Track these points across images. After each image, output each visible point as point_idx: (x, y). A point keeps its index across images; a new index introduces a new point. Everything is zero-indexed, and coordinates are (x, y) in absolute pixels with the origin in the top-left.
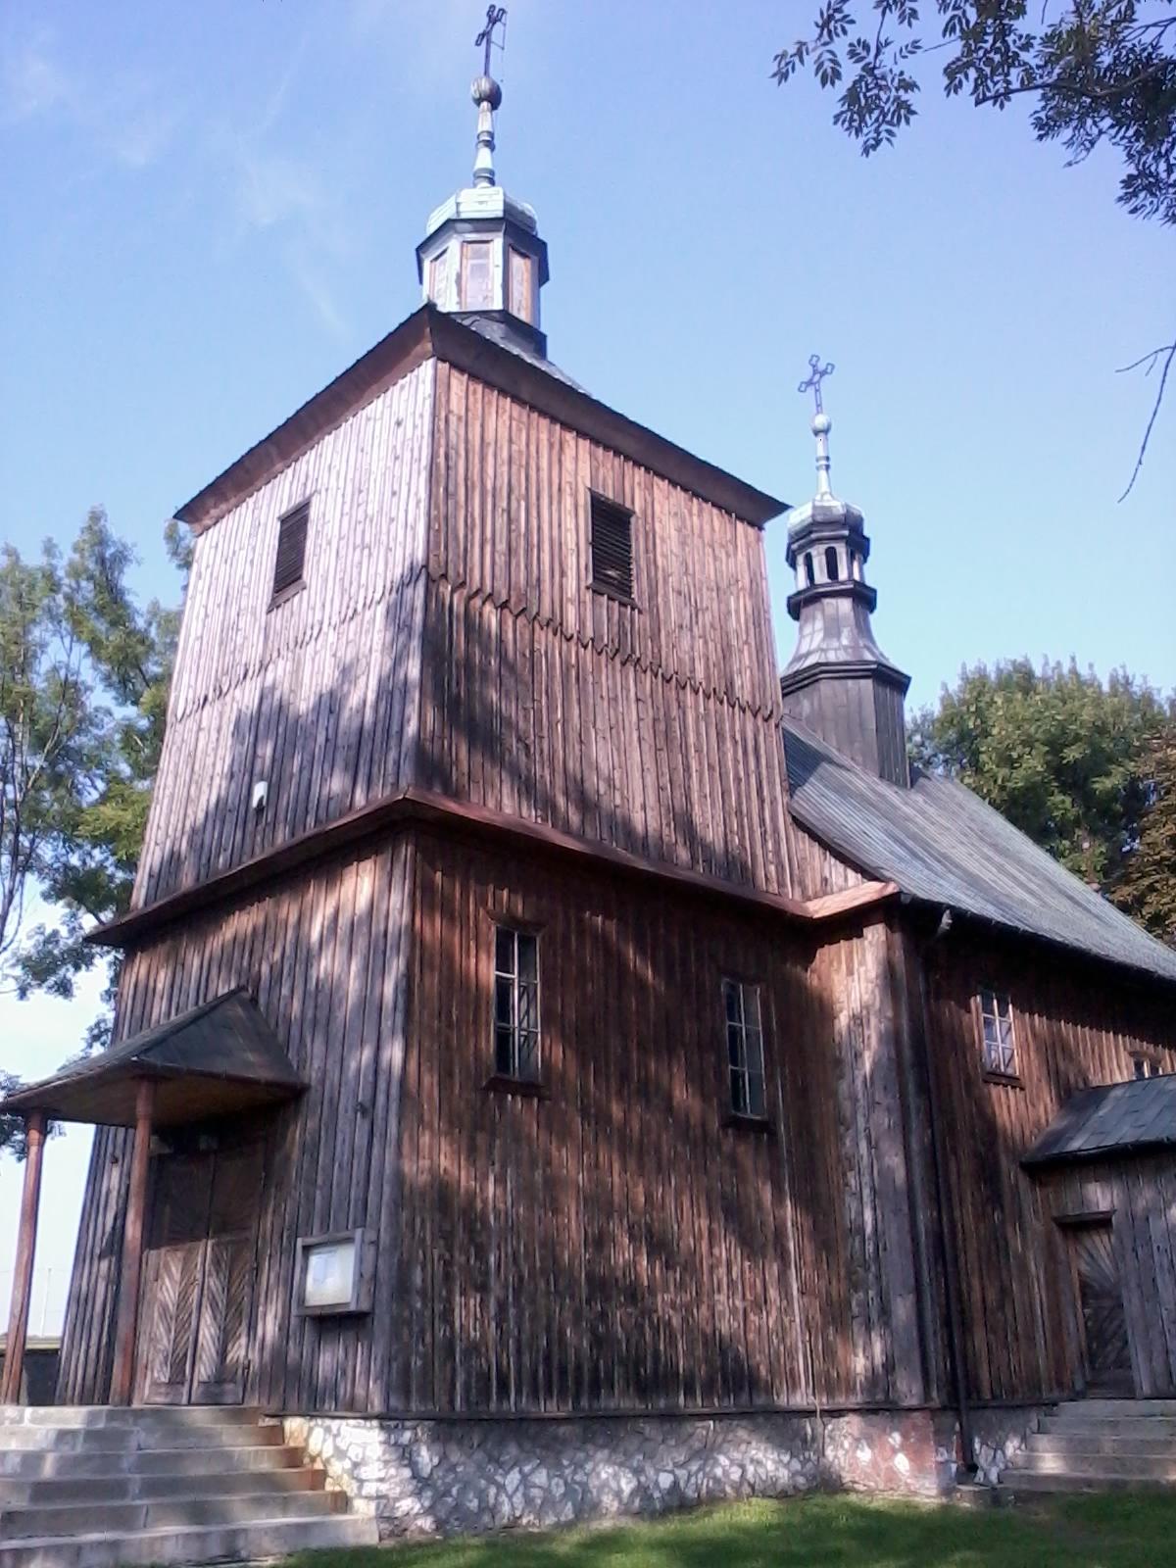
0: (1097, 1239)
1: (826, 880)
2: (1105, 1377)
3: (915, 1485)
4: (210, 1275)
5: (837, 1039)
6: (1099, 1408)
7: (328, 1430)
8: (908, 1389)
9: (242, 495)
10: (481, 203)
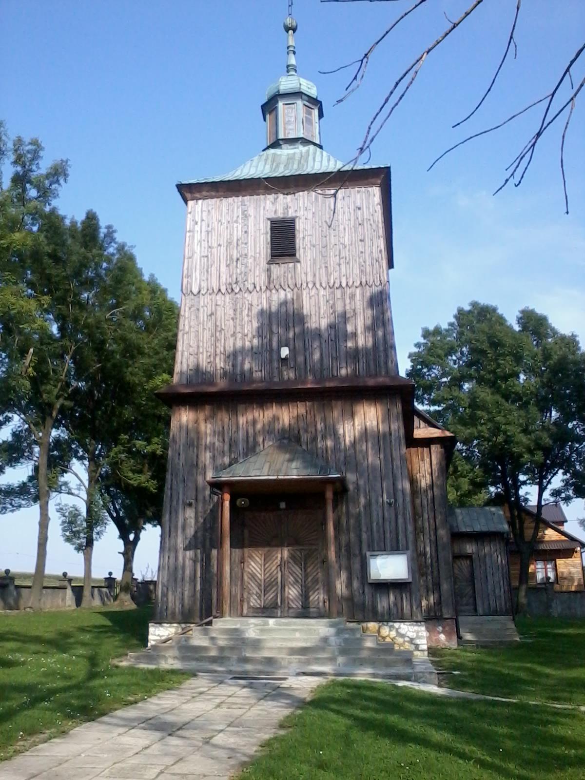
8: (447, 613)
9: (230, 193)
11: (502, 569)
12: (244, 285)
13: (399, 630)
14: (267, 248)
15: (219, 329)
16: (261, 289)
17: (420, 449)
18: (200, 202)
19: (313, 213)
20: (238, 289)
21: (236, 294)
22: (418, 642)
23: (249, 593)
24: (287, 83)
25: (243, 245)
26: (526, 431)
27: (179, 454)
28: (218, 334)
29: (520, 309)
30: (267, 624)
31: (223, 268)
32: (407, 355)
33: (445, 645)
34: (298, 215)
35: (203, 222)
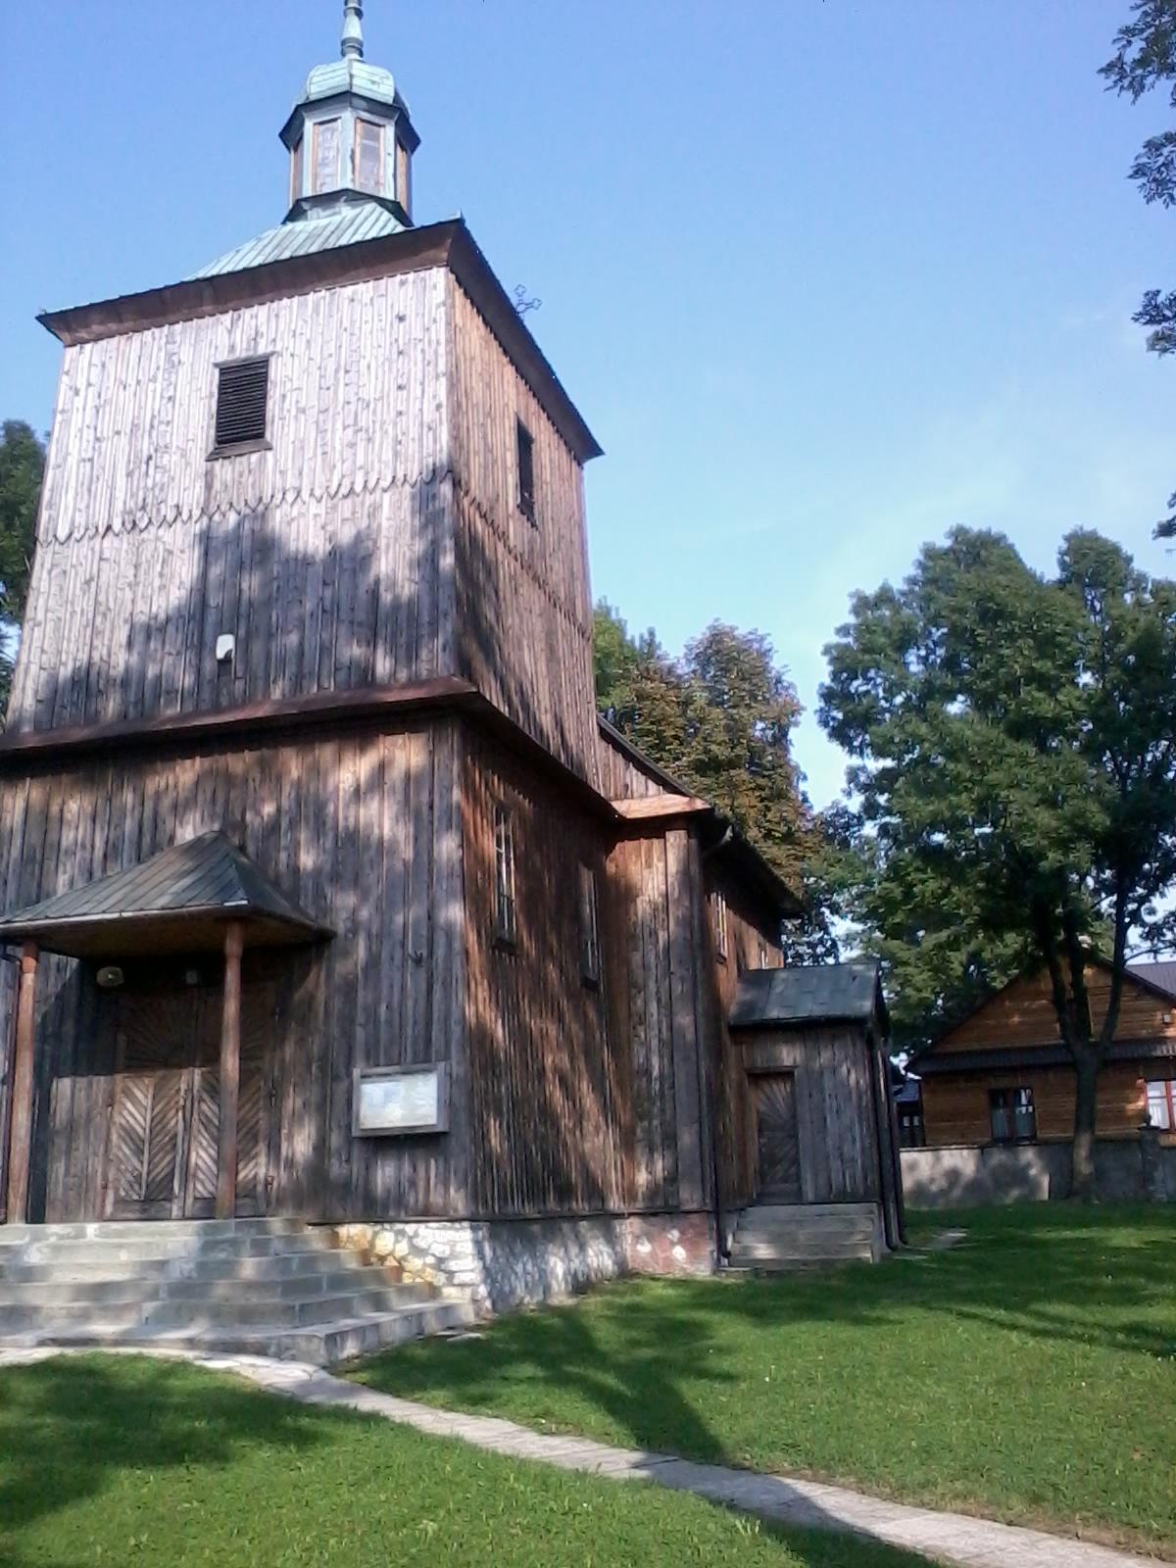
0: (775, 1086)
1: (627, 786)
2: (773, 1188)
3: (690, 1269)
4: (201, 1100)
5: (633, 918)
6: (784, 1211)
7: (402, 1233)
8: (690, 1196)
9: (145, 322)
10: (373, 82)
11: (860, 1098)
12: (158, 510)
13: (415, 1241)
14: (209, 426)
15: (102, 609)
16: (190, 517)
17: (644, 842)
18: (88, 347)
19: (308, 342)
20: (146, 520)
21: (141, 531)
22: (453, 1265)
23: (119, 1170)
24: (323, 80)
25: (163, 427)
26: (1051, 802)
27: (6, 882)
28: (99, 619)
29: (1067, 532)
30: (81, 1234)
31: (121, 481)
32: (821, 649)
33: (683, 1269)
34: (278, 348)
35: (91, 389)
